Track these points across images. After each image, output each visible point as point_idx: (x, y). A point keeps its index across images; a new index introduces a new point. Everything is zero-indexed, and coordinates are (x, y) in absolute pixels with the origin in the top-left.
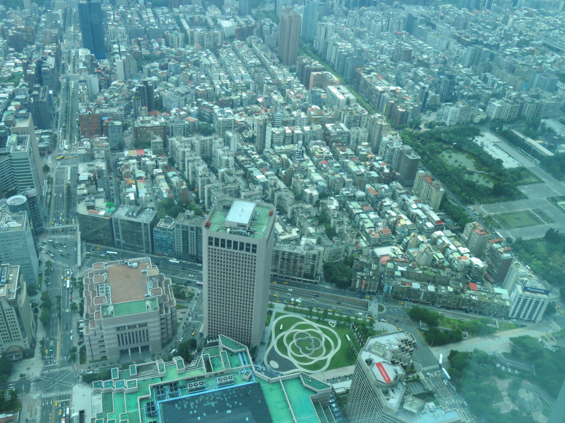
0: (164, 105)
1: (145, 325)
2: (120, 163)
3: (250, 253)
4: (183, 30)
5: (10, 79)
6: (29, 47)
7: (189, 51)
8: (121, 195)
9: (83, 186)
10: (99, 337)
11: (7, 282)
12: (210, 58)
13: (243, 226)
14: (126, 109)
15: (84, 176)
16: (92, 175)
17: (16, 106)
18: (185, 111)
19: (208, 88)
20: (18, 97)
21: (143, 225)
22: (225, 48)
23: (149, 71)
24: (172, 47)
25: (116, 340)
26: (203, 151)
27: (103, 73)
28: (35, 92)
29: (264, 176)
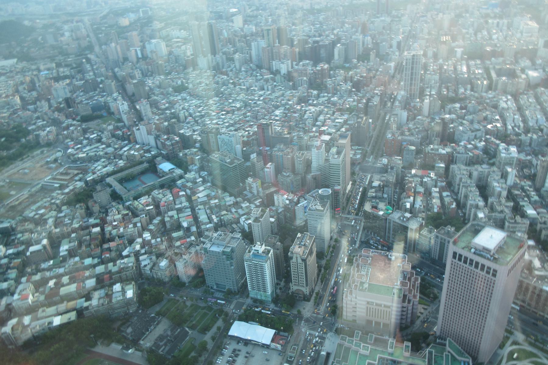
2: (407, 178)
4: (489, 78)
5: (348, 109)
6: (365, 88)
7: (490, 96)
8: (400, 203)
9: (373, 190)
10: (353, 303)
11: (305, 245)
12: (509, 103)
13: (488, 251)
14: (422, 138)
15: (376, 184)
16: (382, 184)
17: (346, 129)
18: (472, 144)
20: (349, 122)
24: (476, 92)
25: (365, 311)
26: (480, 179)
27: (413, 109)
29: (534, 212)
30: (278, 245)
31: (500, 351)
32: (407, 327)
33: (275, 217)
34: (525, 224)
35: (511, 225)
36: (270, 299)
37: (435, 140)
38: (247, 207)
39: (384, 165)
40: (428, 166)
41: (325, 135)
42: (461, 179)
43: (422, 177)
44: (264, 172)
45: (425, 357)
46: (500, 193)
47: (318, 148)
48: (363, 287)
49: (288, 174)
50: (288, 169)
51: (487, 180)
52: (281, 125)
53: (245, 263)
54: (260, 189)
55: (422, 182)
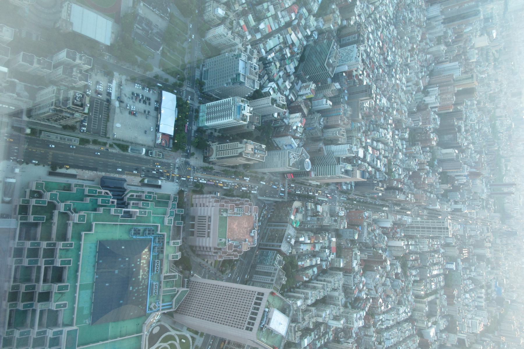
0: (368, 272)
1: (209, 236)
3: (246, 325)
5: (390, 170)
7: (410, 298)
8: (303, 232)
9: (313, 207)
10: (207, 204)
11: (255, 153)
12: (404, 314)
14: (366, 243)
15: (320, 208)
17: (371, 171)
19: (380, 309)
20: (378, 173)
21: (280, 244)
22: (413, 328)
23: (395, 264)
25: (202, 215)
26: (331, 297)
27: (394, 231)
28: (380, 184)
29: (306, 345)
30: (252, 127)
31: (185, 328)
32: (193, 251)
33: (279, 117)
34: (295, 339)
35: (293, 328)
36: (200, 125)
37: (365, 255)
38: (286, 87)
39: (338, 213)
40: (340, 251)
41: (364, 152)
42: (330, 282)
43: (329, 248)
44: (322, 98)
45: (171, 272)
46: (321, 316)
47: (350, 151)
48: (223, 212)
49: (322, 123)
50: (327, 122)
51: (331, 304)
52: (371, 106)
53: (231, 98)
54: (304, 97)
55: (325, 248)
